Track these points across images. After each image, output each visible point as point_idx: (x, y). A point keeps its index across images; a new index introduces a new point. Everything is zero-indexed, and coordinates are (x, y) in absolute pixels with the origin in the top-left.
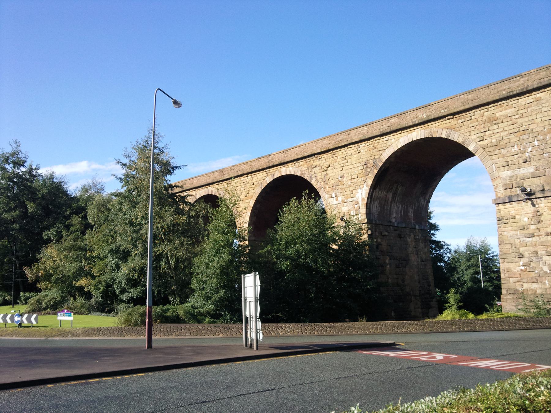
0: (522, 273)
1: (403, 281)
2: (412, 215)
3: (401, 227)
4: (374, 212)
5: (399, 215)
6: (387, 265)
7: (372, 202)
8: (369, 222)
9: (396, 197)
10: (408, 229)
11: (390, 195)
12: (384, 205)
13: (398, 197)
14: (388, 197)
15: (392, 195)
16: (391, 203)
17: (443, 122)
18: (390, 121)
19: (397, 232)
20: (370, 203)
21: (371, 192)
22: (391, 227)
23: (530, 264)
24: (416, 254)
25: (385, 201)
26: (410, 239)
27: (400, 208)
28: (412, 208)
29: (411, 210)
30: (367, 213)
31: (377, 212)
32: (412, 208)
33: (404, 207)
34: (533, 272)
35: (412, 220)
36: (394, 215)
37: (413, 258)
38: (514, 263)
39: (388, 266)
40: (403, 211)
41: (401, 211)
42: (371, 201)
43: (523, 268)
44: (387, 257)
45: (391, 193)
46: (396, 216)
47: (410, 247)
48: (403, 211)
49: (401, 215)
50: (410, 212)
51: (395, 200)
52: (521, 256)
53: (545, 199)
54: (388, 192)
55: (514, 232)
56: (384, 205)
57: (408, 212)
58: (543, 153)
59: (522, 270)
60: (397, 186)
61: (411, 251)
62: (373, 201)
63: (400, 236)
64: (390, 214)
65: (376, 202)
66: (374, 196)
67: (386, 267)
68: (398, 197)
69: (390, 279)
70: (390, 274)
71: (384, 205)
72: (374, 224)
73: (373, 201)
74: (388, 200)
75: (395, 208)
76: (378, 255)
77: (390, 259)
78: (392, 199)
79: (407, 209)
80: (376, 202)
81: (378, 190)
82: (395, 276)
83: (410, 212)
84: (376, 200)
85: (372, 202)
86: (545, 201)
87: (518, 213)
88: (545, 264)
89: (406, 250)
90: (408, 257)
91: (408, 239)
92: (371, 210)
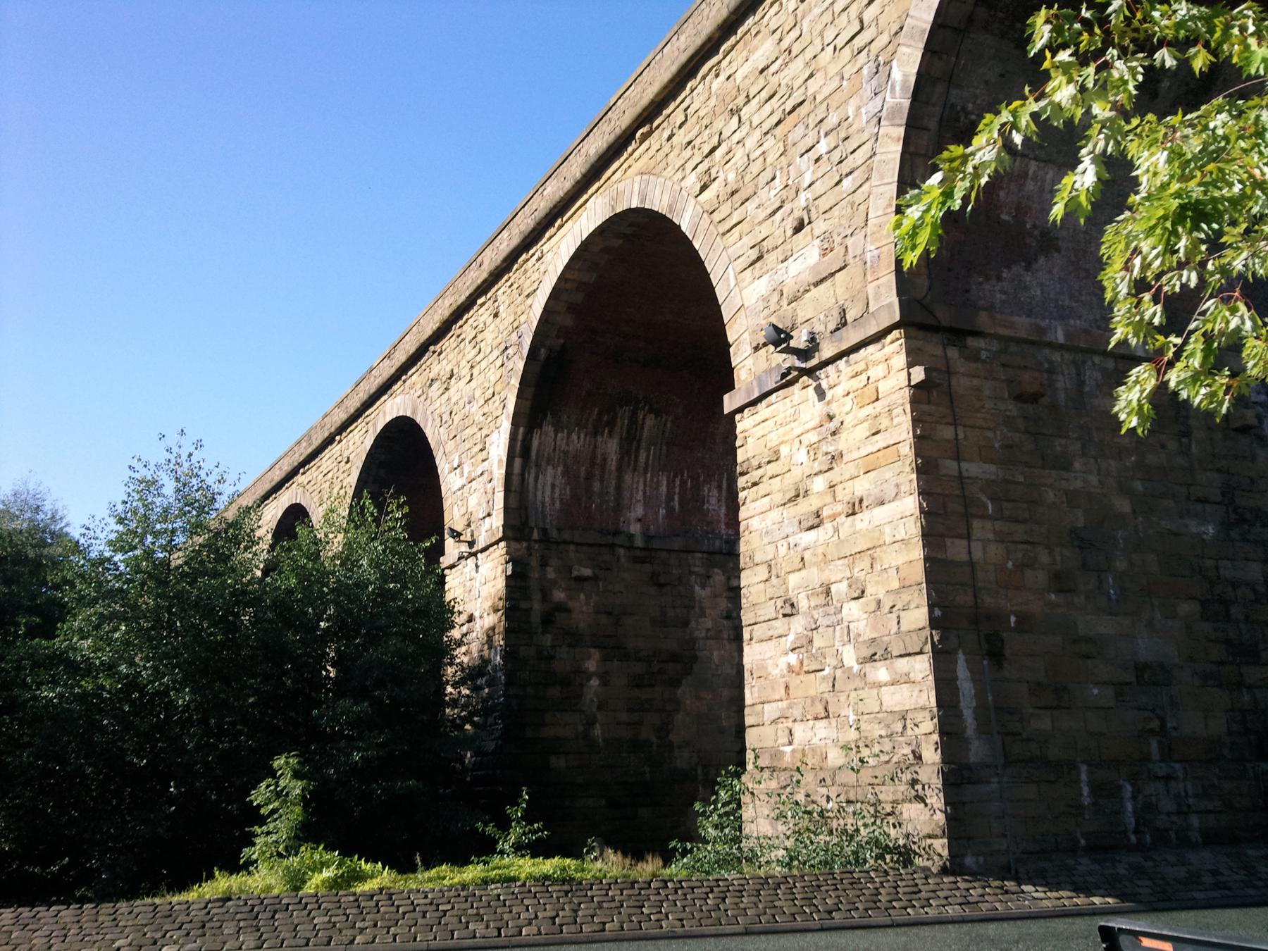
0: (794, 681)
1: (663, 730)
2: (723, 510)
3: (670, 551)
4: (543, 503)
5: (662, 512)
6: (589, 679)
7: (533, 471)
8: (510, 534)
9: (637, 451)
10: (699, 555)
11: (611, 447)
12: (586, 479)
13: (648, 451)
14: (599, 451)
15: (621, 446)
16: (620, 469)
17: (636, 154)
18: (545, 193)
19: (648, 568)
20: (522, 475)
21: (520, 437)
22: (622, 551)
23: (811, 641)
24: (729, 639)
25: (593, 464)
26: (708, 590)
27: (664, 489)
28: (719, 487)
29: (715, 492)
30: (514, 504)
31: (558, 505)
32: (719, 487)
33: (683, 483)
34: (818, 674)
35: (723, 527)
36: (639, 511)
37: (715, 653)
38: (774, 640)
39: (595, 682)
40: (676, 498)
41: (670, 498)
42: (525, 466)
43: (793, 658)
44: (593, 650)
45: (611, 434)
46: (645, 516)
47: (703, 615)
48: (676, 498)
49: (670, 510)
50: (713, 501)
51: (636, 460)
52: (788, 610)
53: (847, 362)
54: (595, 434)
55: (775, 515)
56: (589, 477)
57: (700, 500)
58: (837, 179)
59: (791, 669)
60: (634, 414)
61: (708, 630)
62: (538, 465)
63: (656, 581)
64: (619, 507)
65: (550, 470)
66: (538, 451)
67: (581, 685)
68: (648, 451)
69: (598, 726)
70: (599, 708)
71: (589, 477)
72: (536, 541)
73: (538, 465)
74: (605, 460)
75: (641, 487)
76: (549, 643)
77: (605, 659)
78: (622, 458)
79: (697, 487)
80: (550, 470)
81: (549, 428)
82: (624, 717)
83: (713, 501)
84: (548, 464)
85: (533, 471)
86: (849, 369)
87: (784, 435)
88: (846, 639)
89: (686, 624)
90: (693, 649)
91: (697, 588)
92: (531, 495)
